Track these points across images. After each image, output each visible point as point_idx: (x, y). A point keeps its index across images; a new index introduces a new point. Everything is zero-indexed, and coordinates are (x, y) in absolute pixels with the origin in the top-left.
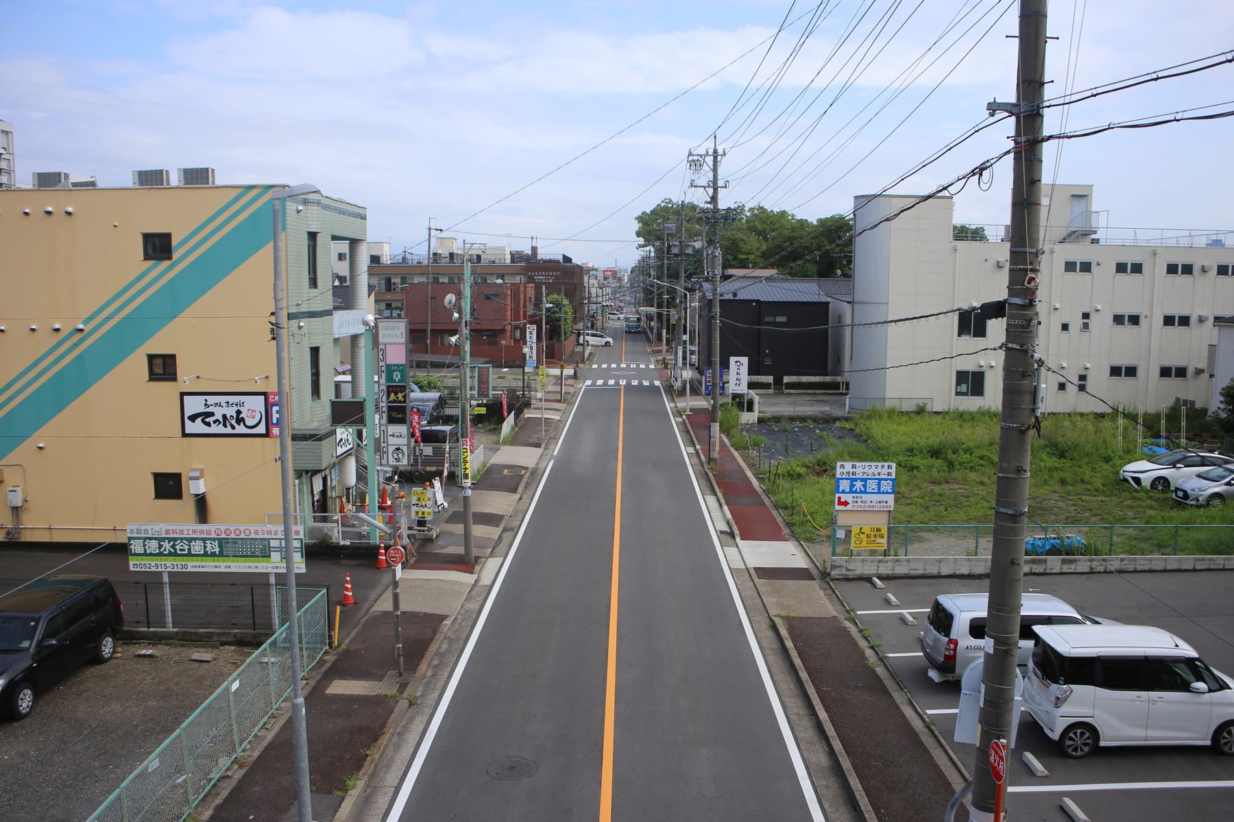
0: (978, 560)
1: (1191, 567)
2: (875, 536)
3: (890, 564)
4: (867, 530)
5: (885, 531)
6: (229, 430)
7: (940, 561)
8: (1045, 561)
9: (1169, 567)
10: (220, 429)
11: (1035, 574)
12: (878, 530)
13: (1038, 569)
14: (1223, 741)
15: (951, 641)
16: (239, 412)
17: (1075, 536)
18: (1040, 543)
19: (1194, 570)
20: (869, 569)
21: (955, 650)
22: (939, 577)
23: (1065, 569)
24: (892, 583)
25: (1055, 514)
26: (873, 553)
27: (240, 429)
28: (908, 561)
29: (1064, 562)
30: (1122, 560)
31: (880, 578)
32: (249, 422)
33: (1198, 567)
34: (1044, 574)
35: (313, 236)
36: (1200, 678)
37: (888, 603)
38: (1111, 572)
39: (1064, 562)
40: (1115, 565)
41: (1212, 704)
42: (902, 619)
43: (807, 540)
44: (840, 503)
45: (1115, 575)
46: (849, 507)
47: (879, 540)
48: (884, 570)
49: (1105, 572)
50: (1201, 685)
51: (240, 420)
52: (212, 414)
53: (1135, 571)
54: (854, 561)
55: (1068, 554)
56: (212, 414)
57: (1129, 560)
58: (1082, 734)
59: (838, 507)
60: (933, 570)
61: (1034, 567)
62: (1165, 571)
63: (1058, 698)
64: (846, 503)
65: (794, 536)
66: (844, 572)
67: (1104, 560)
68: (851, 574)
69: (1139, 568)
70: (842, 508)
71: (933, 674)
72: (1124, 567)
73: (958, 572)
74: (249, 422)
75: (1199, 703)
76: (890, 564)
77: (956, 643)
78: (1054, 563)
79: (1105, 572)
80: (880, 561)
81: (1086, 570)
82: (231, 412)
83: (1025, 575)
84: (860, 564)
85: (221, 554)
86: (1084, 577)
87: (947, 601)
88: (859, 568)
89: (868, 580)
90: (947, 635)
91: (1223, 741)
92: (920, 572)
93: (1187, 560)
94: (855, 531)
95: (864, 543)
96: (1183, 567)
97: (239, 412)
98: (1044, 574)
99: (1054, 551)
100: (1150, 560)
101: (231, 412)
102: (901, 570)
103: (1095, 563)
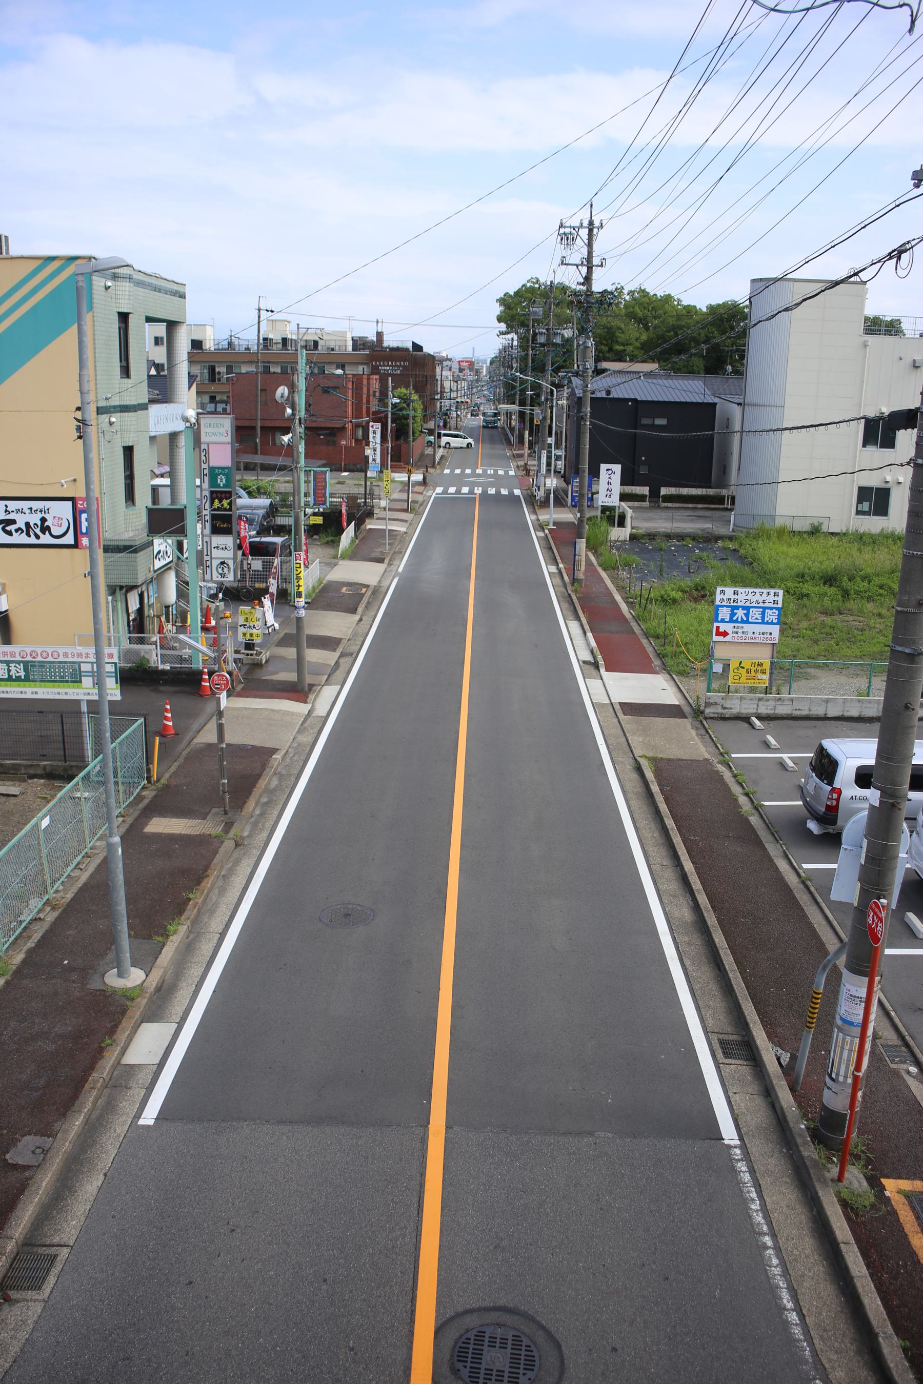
0: (870, 702)
2: (756, 671)
3: (771, 703)
4: (747, 664)
6: (33, 540)
7: (827, 701)
10: (22, 539)
12: (760, 664)
15: (834, 790)
16: (43, 520)
20: (748, 708)
21: (838, 800)
22: (825, 718)
24: (772, 723)
26: (752, 690)
27: (46, 539)
28: (792, 700)
31: (760, 718)
32: (56, 531)
35: (124, 317)
37: (767, 746)
42: (782, 765)
43: (681, 674)
44: (718, 633)
47: (760, 676)
48: (764, 710)
51: (45, 529)
52: (13, 522)
54: (732, 698)
56: (13, 522)
59: (715, 638)
60: (819, 711)
64: (725, 634)
66: (720, 710)
68: (727, 713)
70: (721, 638)
71: (812, 826)
73: (846, 714)
74: (56, 531)
76: (771, 703)
77: (839, 792)
80: (760, 699)
82: (35, 519)
85: (27, 679)
88: (736, 706)
89: (746, 719)
90: (830, 783)
92: (805, 713)
94: (734, 665)
95: (743, 679)
97: (43, 520)
101: (35, 519)
102: (783, 710)
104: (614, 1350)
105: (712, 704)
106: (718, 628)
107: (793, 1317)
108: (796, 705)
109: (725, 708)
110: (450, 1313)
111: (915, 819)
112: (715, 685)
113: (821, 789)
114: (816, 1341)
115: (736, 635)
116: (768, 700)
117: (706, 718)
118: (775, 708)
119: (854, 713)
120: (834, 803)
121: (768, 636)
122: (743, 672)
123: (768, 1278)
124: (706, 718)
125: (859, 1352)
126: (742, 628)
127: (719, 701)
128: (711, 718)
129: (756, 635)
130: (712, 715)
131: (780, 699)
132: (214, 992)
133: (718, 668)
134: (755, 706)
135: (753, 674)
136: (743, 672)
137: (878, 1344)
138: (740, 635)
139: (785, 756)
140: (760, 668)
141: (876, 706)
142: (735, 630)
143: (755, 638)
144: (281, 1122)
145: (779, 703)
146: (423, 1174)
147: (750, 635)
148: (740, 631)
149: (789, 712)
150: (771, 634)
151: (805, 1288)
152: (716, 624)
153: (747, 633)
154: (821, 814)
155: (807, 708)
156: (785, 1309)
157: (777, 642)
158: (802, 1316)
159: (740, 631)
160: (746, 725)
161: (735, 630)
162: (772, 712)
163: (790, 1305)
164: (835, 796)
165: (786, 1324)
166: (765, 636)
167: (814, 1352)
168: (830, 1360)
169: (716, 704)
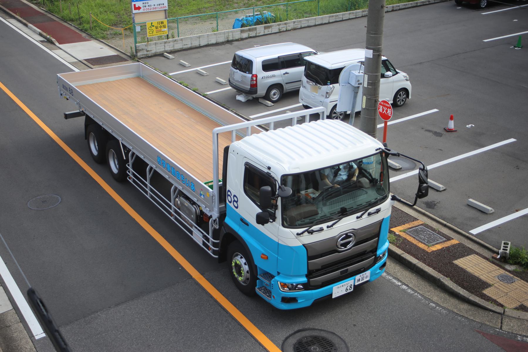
0: (220, 34)
1: (327, 22)
2: (161, 27)
3: (172, 43)
4: (155, 24)
5: (166, 23)
7: (199, 37)
8: (256, 29)
9: (317, 23)
11: (251, 37)
12: (162, 23)
13: (252, 34)
14: (398, 100)
15: (253, 76)
17: (268, 14)
18: (250, 19)
19: (329, 23)
20: (160, 49)
21: (256, 80)
22: (200, 47)
23: (267, 32)
24: (176, 54)
25: (237, 3)
26: (160, 38)
28: (182, 40)
29: (265, 28)
30: (294, 22)
31: (171, 52)
33: (331, 21)
34: (256, 37)
36: (388, 70)
37: (183, 66)
38: (289, 30)
39: (265, 28)
40: (291, 26)
41: (393, 82)
42: (198, 73)
43: (103, 38)
44: (136, 8)
45: (292, 31)
46: (141, 10)
47: (163, 29)
48: (169, 48)
49: (286, 31)
50: (389, 73)
53: (301, 28)
54: (150, 45)
55: (266, 23)
57: (298, 22)
58: (400, 95)
59: (134, 11)
60: (196, 43)
61: (250, 33)
62: (315, 25)
63: (327, 93)
64: (139, 8)
65: (92, 37)
66: (145, 53)
67: (285, 24)
68: (150, 54)
69: (303, 26)
70: (137, 11)
71: (241, 98)
72: (295, 26)
73: (210, 43)
75: (388, 83)
76: (172, 43)
77: (256, 76)
78: (260, 29)
79: (286, 31)
80: (165, 43)
81: (277, 31)
83: (387, 12)
84: (154, 46)
86: (278, 35)
87: (246, 53)
88: (154, 49)
89: (161, 55)
90: (251, 73)
91: (398, 100)
92: (189, 46)
93: (326, 18)
94: (148, 25)
95: (155, 33)
96: (324, 22)
98: (256, 37)
99: (259, 22)
100: (308, 20)
102: (178, 46)
103: (281, 26)
104: (354, 325)
105: (141, 50)
106: (135, 5)
107: (404, 287)
108: (185, 42)
109: (148, 51)
110: (281, 343)
111: (301, 81)
112: (139, 39)
113: (246, 77)
114: (419, 291)
115: (145, 8)
116: (169, 42)
117: (139, 59)
118: (174, 46)
119: (213, 41)
120: (255, 82)
121: (162, 6)
122: (154, 28)
123: (384, 278)
124: (139, 59)
125: (435, 289)
126: (148, 3)
127: (144, 47)
128: (143, 58)
129: (156, 6)
130: (142, 56)
131: (175, 41)
132: (6, 263)
133: (138, 29)
134: (163, 47)
135: (159, 29)
136: (154, 28)
137: (442, 282)
138: (147, 7)
139: (198, 69)
140: (162, 25)
141: (223, 35)
142: (144, 5)
143: (156, 8)
144: (117, 305)
145: (175, 43)
146: (212, 297)
147: (153, 7)
148: (147, 5)
149: (181, 47)
150: (163, 4)
151: (399, 275)
152: (133, 3)
153: (151, 6)
154: (248, 90)
155: (190, 43)
156: (399, 286)
157: (167, 8)
158: (407, 286)
159: (147, 5)
160: (163, 58)
161: (144, 5)
162: (172, 48)
163: (400, 284)
164: (254, 78)
165: (403, 290)
166: (161, 6)
167: (421, 295)
168: (429, 296)
169: (143, 49)
